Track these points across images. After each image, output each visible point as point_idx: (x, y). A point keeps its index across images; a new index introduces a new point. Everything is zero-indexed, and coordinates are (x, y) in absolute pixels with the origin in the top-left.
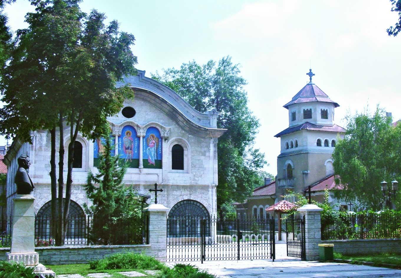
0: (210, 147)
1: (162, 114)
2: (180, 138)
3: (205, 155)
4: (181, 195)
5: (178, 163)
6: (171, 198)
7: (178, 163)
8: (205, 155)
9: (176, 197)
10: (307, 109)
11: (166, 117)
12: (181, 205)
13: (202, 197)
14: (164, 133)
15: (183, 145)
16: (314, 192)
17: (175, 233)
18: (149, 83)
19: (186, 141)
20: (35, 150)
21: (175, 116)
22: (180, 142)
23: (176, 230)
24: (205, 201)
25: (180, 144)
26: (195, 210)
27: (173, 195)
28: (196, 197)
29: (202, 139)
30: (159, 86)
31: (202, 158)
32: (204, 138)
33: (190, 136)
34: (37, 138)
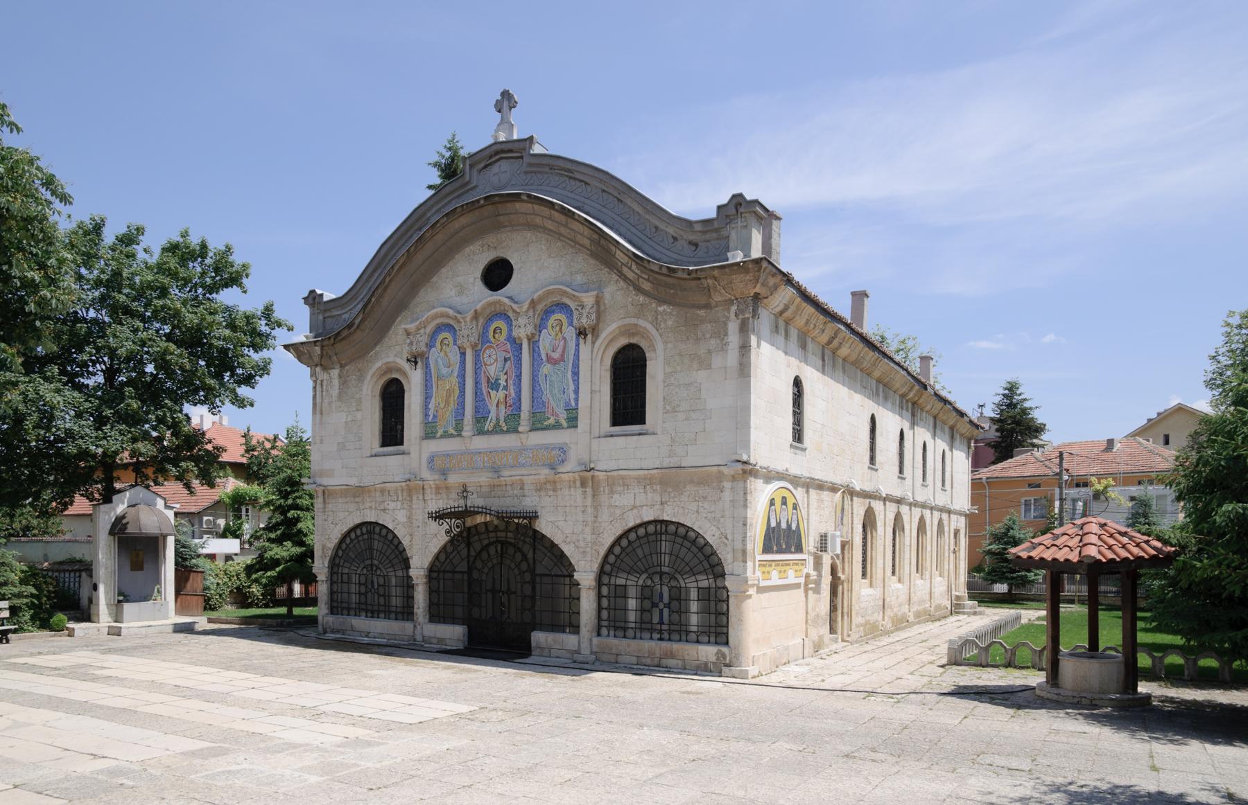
0: (726, 334)
1: (580, 258)
2: (633, 321)
3: (709, 367)
4: (634, 507)
5: (628, 405)
6: (604, 516)
7: (628, 405)
8: (709, 367)
9: (618, 512)
10: (321, 295)
11: (592, 261)
12: (676, 534)
13: (701, 510)
14: (581, 314)
15: (643, 344)
16: (247, 511)
17: (622, 624)
18: (547, 169)
19: (649, 327)
20: (321, 413)
21: (608, 251)
22: (633, 334)
23: (688, 619)
24: (708, 525)
25: (634, 341)
26: (681, 555)
27: (610, 506)
28: (681, 511)
29: (702, 313)
30: (570, 171)
31: (702, 375)
32: (707, 306)
33: (661, 309)
34: (781, 307)
